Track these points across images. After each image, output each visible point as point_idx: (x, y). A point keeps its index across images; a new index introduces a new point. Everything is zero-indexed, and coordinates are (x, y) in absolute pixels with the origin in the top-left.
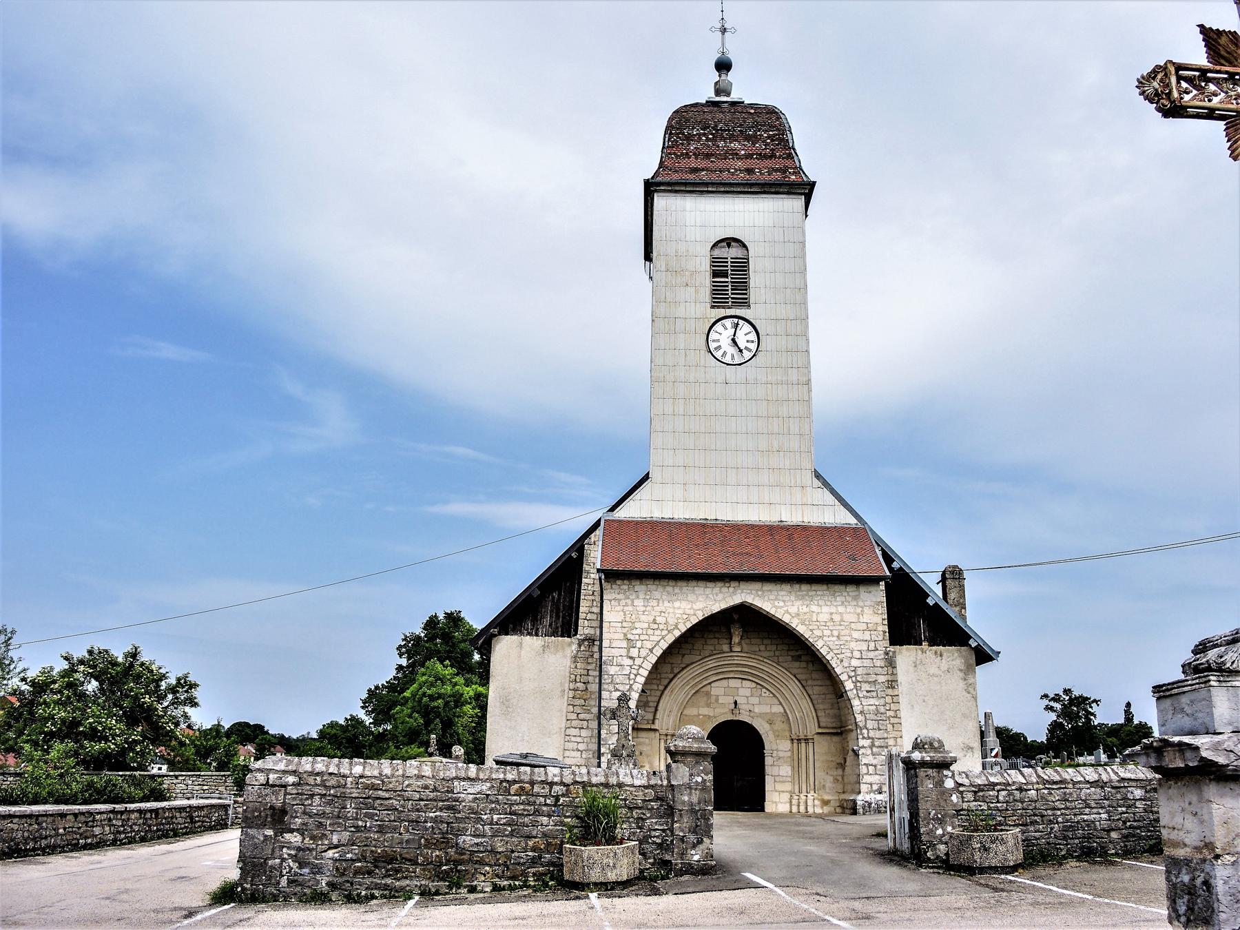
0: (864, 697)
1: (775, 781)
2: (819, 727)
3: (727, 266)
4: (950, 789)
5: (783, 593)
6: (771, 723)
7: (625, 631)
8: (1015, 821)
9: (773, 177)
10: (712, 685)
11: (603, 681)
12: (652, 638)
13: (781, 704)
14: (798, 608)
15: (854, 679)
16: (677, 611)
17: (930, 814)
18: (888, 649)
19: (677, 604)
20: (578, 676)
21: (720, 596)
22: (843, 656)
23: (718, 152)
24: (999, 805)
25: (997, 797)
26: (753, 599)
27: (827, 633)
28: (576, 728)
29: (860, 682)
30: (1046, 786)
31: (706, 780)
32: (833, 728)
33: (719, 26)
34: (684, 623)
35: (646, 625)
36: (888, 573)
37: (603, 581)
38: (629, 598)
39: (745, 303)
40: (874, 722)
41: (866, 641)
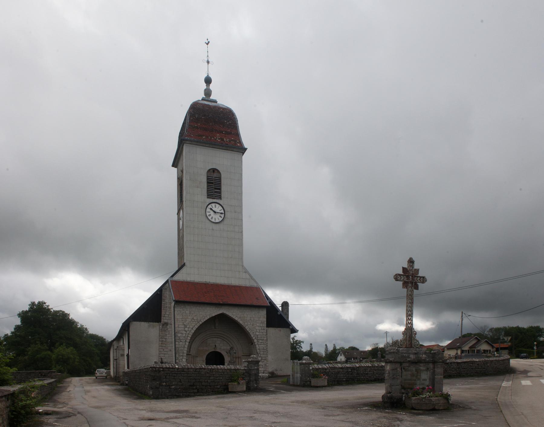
2: (243, 353)
3: (213, 181)
4: (311, 369)
19: (201, 313)
20: (163, 338)
28: (163, 354)
29: (259, 340)
33: (206, 60)
35: (190, 320)
36: (269, 305)
39: (220, 198)
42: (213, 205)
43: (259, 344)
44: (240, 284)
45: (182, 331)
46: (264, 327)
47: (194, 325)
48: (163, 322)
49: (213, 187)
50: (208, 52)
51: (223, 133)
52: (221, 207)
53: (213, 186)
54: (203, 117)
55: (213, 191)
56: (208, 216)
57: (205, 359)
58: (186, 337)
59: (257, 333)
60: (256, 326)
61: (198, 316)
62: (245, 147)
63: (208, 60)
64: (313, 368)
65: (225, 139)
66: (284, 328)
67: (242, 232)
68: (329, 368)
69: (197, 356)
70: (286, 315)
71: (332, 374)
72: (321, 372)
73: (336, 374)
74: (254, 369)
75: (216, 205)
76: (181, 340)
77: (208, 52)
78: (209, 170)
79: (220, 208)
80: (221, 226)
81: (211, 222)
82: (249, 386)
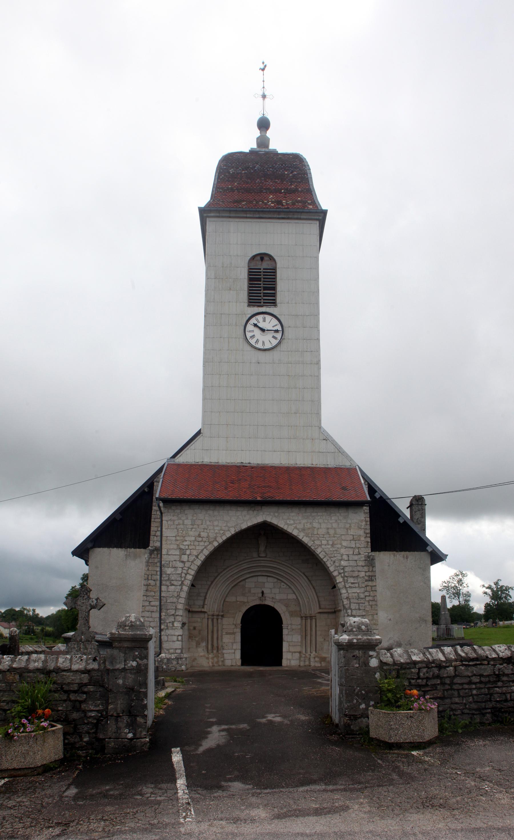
0: (350, 587)
1: (289, 646)
2: (320, 608)
3: (260, 275)
5: (293, 514)
6: (287, 606)
7: (178, 543)
8: (433, 695)
9: (296, 206)
10: (247, 580)
11: (162, 579)
12: (197, 548)
13: (294, 593)
14: (304, 525)
15: (343, 575)
16: (216, 528)
17: (355, 690)
18: (370, 554)
19: (216, 523)
20: (150, 578)
21: (248, 517)
22: (335, 558)
23: (255, 187)
24: (419, 681)
25: (418, 673)
26: (272, 519)
27: (324, 542)
28: (148, 612)
29: (347, 577)
30: (464, 663)
31: (140, 664)
32: (328, 609)
33: (261, 93)
34: (221, 537)
35: (193, 539)
36: (369, 499)
37: (162, 509)
38: (181, 519)
39: (274, 303)
40: (356, 604)
41: (352, 548)
42: (260, 317)
43: (347, 586)
44: (314, 463)
45: (174, 562)
46: (358, 548)
47: (201, 548)
48: (152, 547)
49: (260, 287)
50: (264, 81)
51: (281, 193)
52: (276, 320)
53: (260, 284)
54: (243, 172)
55: (260, 293)
56: (248, 338)
57: (239, 621)
58: (183, 575)
59: (343, 563)
60: (339, 546)
61: (210, 530)
62: (324, 208)
63: (264, 93)
64: (382, 663)
65: (284, 201)
66: (414, 550)
67: (318, 363)
68: (456, 660)
69: (222, 616)
70: (419, 524)
71: (470, 683)
72: (419, 678)
73: (486, 683)
74: (124, 670)
75: (265, 318)
76: (173, 580)
77: (264, 81)
78: (253, 258)
79: (275, 322)
80: (275, 354)
81: (254, 349)
82: (101, 736)
